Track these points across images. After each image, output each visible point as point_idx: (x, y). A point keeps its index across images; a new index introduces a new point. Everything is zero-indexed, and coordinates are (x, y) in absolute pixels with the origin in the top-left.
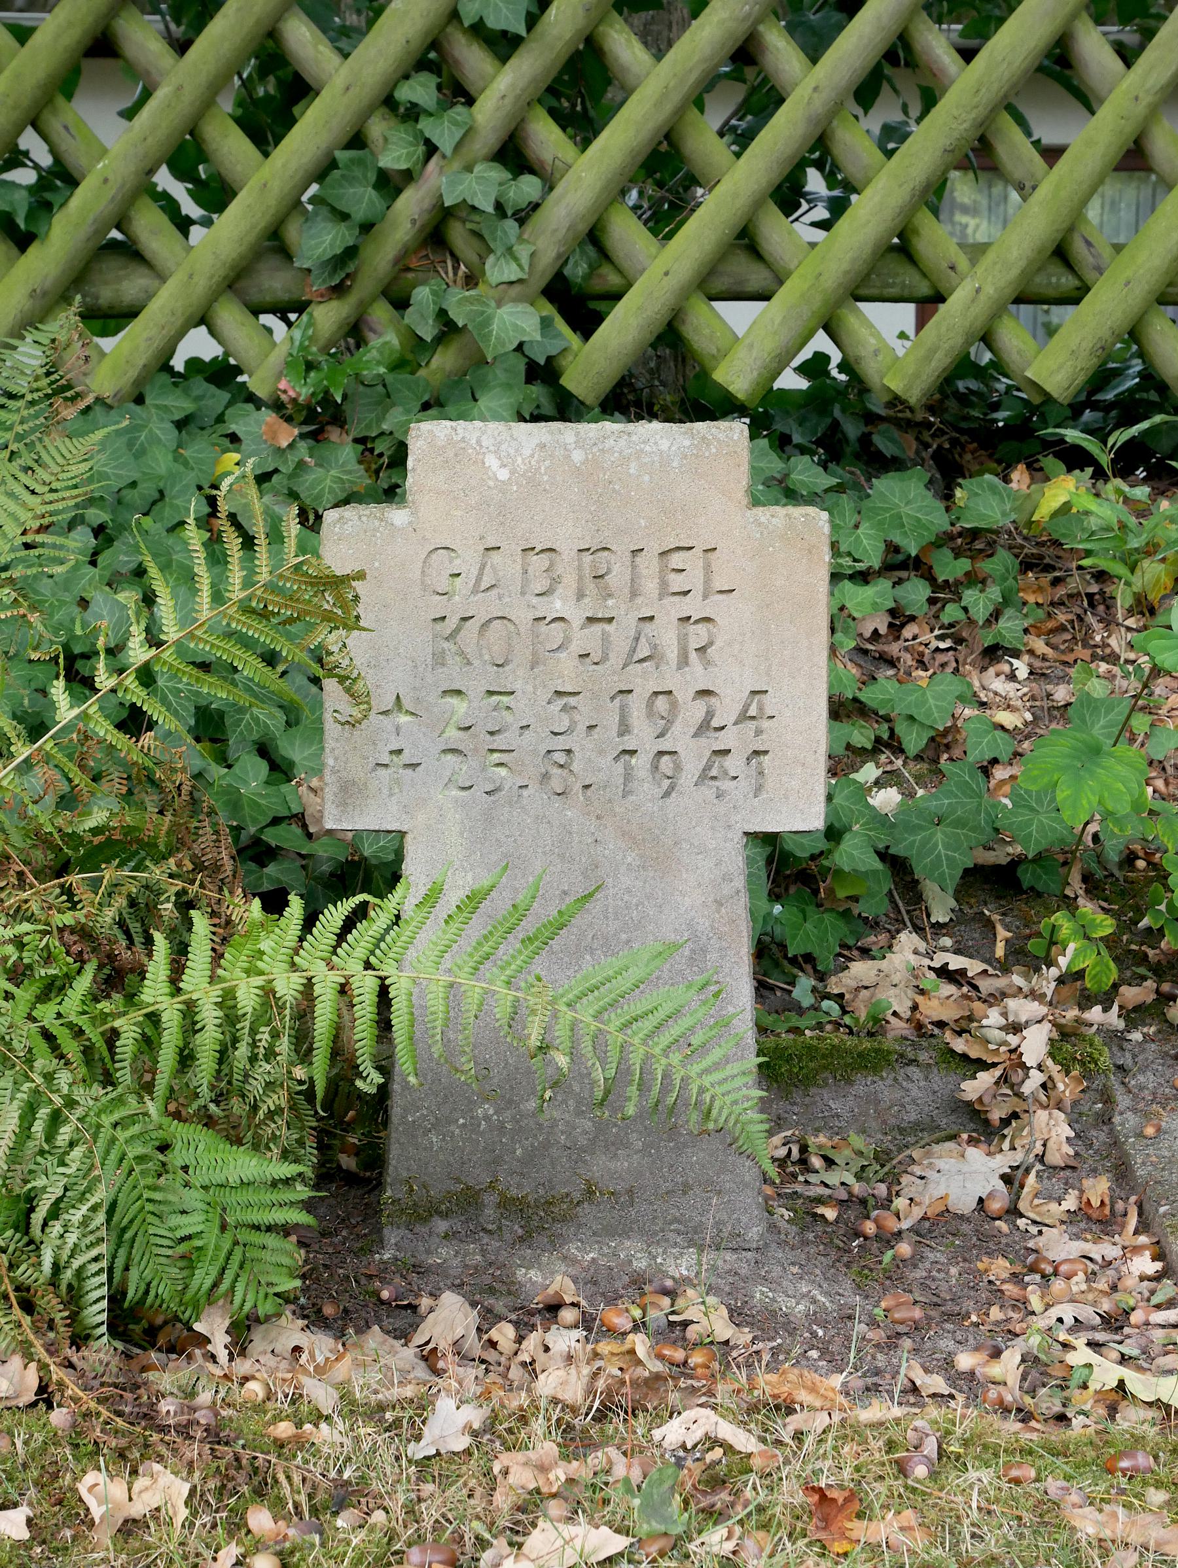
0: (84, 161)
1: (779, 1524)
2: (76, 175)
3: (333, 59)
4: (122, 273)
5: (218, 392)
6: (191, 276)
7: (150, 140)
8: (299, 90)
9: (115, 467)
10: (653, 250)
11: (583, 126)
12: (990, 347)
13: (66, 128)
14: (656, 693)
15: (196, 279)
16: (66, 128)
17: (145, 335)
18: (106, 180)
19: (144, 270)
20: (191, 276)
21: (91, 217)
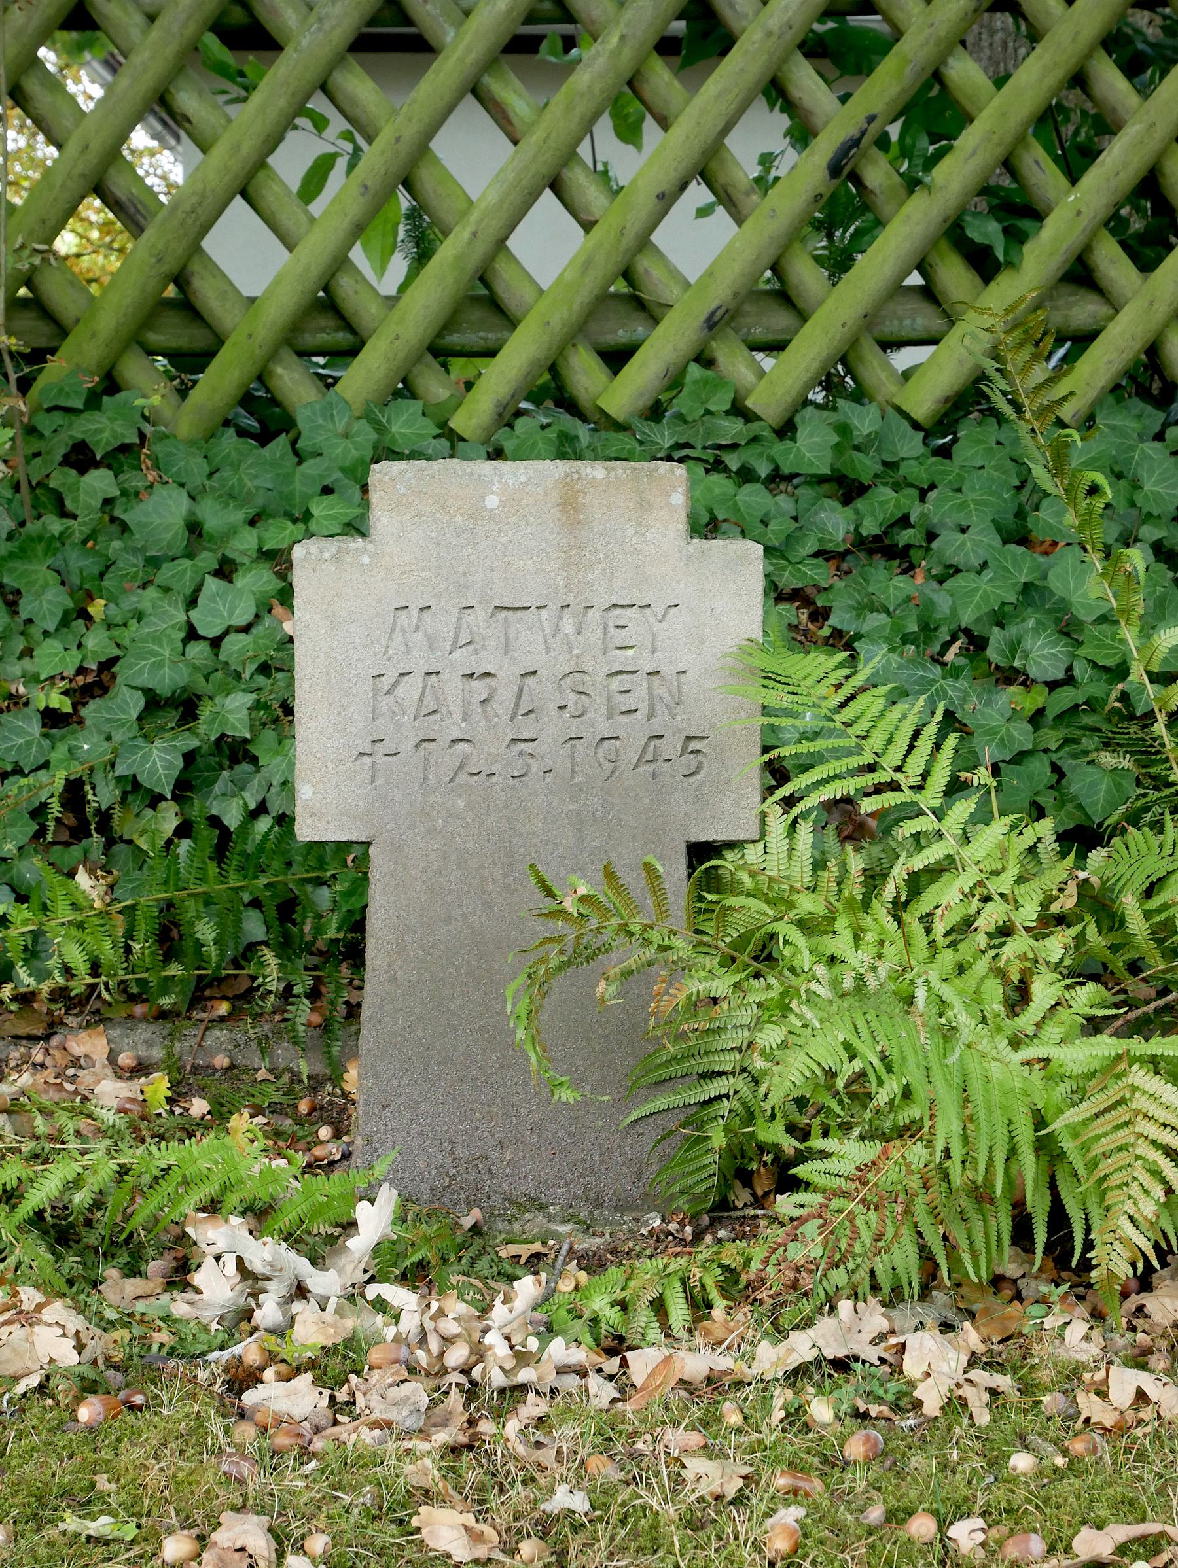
0: (1051, 195)
1: (539, 1445)
2: (1040, 207)
3: (1133, 99)
4: (1072, 299)
5: (1155, 412)
6: (1151, 303)
7: (1122, 174)
8: (1106, 125)
9: (1167, 487)
10: (1139, 282)
11: (1075, 162)
12: (683, 371)
13: (1037, 162)
14: (428, 674)
15: (1156, 306)
16: (1037, 162)
17: (1105, 359)
18: (1079, 213)
19: (1094, 297)
20: (1151, 303)
21: (1065, 246)
